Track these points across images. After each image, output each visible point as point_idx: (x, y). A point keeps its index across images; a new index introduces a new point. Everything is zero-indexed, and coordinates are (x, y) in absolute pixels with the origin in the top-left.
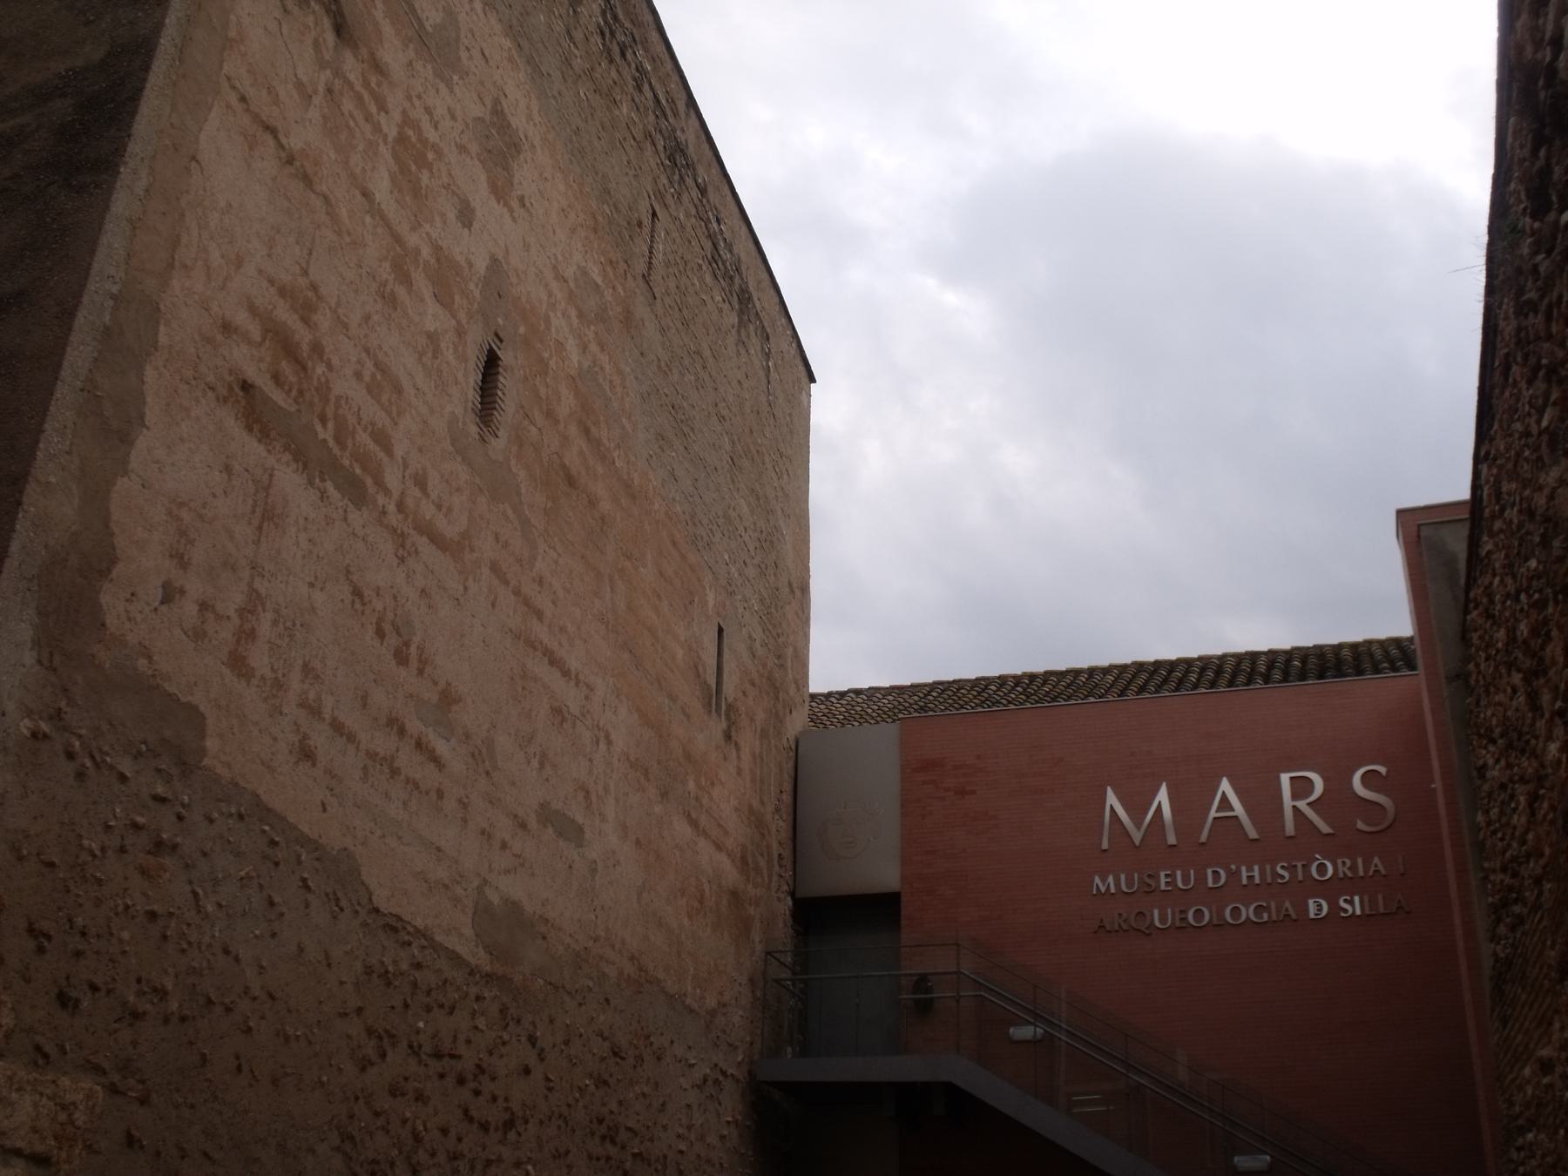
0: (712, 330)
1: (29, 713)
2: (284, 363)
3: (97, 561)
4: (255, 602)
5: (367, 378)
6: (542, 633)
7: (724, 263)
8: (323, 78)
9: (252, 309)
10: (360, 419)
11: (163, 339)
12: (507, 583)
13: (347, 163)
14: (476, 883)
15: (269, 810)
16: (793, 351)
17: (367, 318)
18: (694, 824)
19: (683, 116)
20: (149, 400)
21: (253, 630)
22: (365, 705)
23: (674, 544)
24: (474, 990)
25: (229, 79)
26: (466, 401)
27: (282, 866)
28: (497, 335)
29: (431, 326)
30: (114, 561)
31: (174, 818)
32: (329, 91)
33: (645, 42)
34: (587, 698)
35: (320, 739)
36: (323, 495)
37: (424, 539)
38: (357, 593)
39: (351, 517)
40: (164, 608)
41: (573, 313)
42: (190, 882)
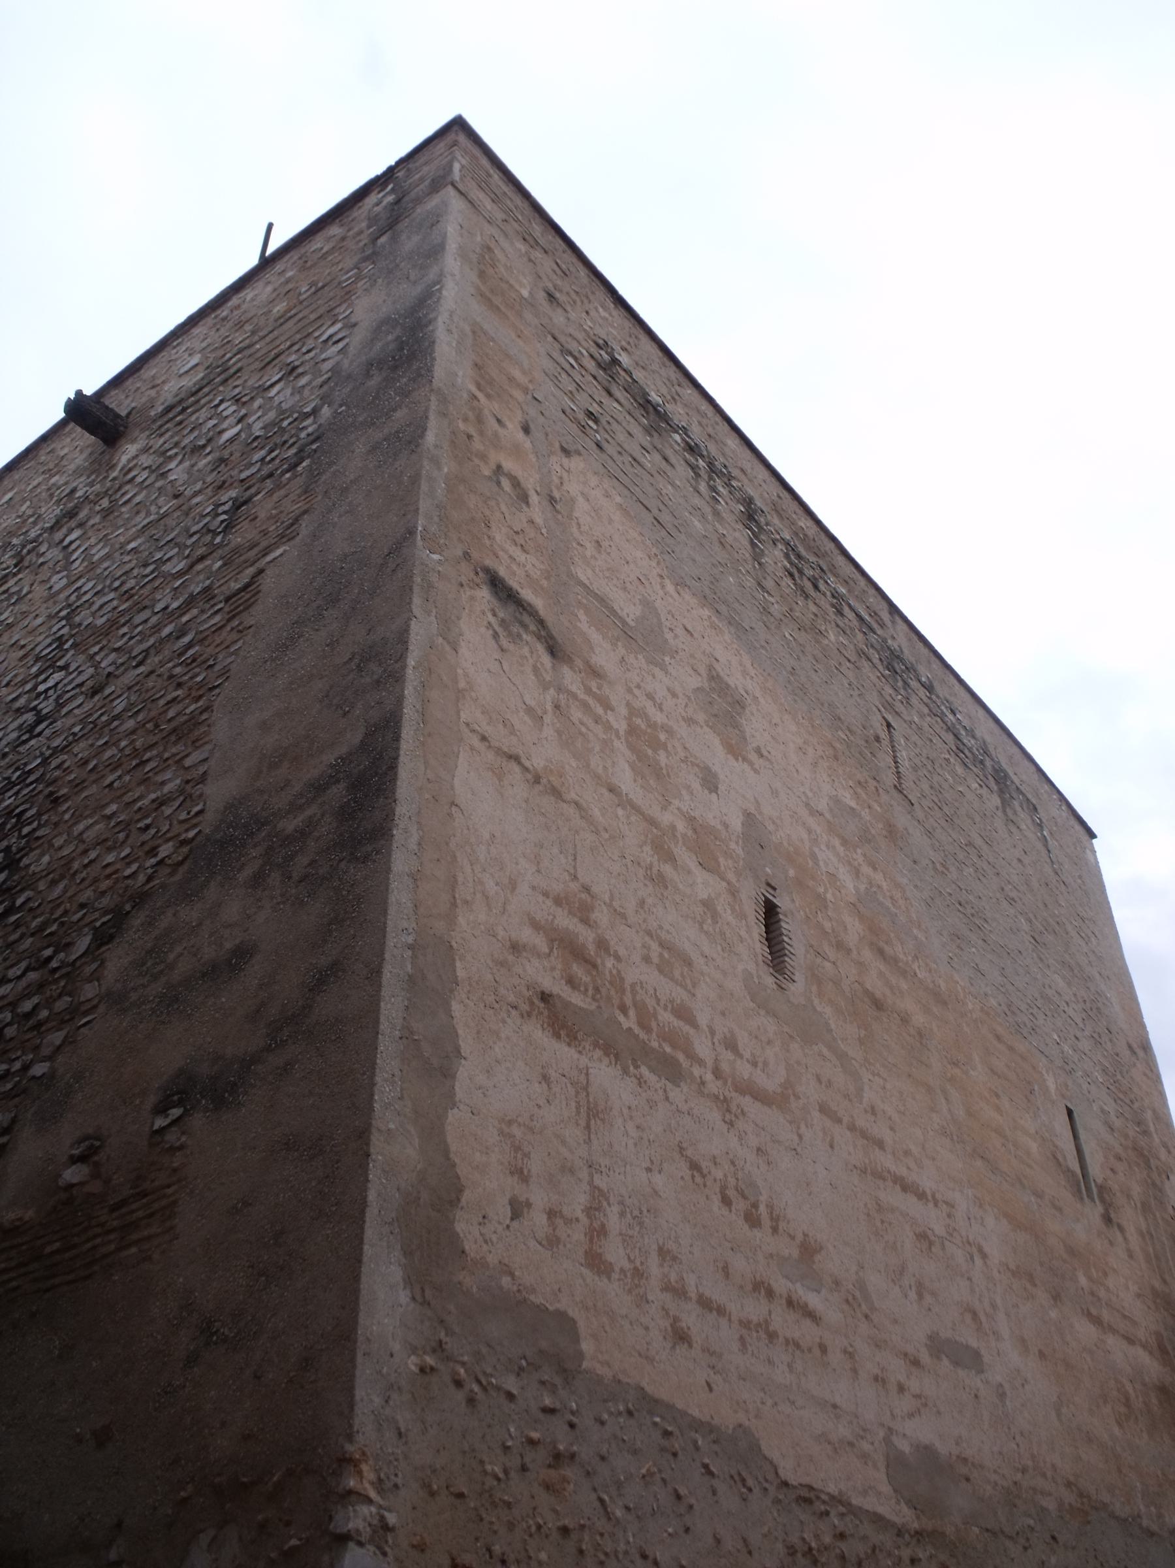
0: (977, 819)
1: (414, 1350)
2: (575, 967)
3: (442, 1193)
4: (597, 1201)
5: (656, 960)
6: (886, 1161)
7: (970, 750)
8: (548, 698)
9: (536, 925)
10: (658, 1001)
11: (461, 973)
12: (840, 1121)
13: (588, 765)
14: (882, 1434)
15: (656, 1401)
16: (1065, 813)
17: (642, 903)
18: (1097, 1321)
19: (889, 624)
20: (460, 1032)
21: (603, 1226)
22: (727, 1275)
23: (998, 1038)
24: (906, 1554)
25: (467, 725)
26: (756, 955)
27: (681, 1456)
28: (769, 885)
29: (703, 895)
30: (460, 1190)
31: (566, 1428)
32: (557, 707)
33: (833, 569)
34: (949, 1216)
35: (691, 1318)
36: (641, 1082)
37: (748, 1099)
38: (694, 1166)
39: (671, 1095)
40: (515, 1224)
41: (837, 842)
42: (595, 1490)
